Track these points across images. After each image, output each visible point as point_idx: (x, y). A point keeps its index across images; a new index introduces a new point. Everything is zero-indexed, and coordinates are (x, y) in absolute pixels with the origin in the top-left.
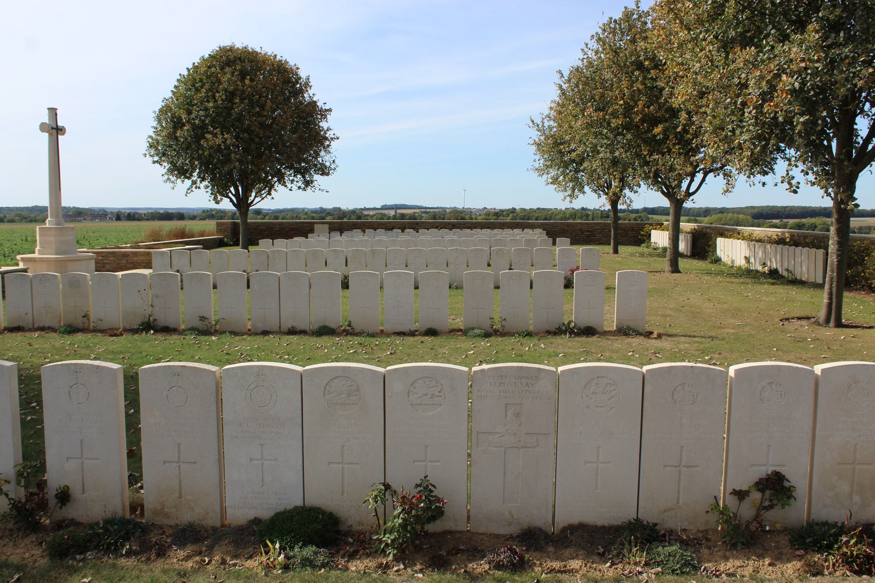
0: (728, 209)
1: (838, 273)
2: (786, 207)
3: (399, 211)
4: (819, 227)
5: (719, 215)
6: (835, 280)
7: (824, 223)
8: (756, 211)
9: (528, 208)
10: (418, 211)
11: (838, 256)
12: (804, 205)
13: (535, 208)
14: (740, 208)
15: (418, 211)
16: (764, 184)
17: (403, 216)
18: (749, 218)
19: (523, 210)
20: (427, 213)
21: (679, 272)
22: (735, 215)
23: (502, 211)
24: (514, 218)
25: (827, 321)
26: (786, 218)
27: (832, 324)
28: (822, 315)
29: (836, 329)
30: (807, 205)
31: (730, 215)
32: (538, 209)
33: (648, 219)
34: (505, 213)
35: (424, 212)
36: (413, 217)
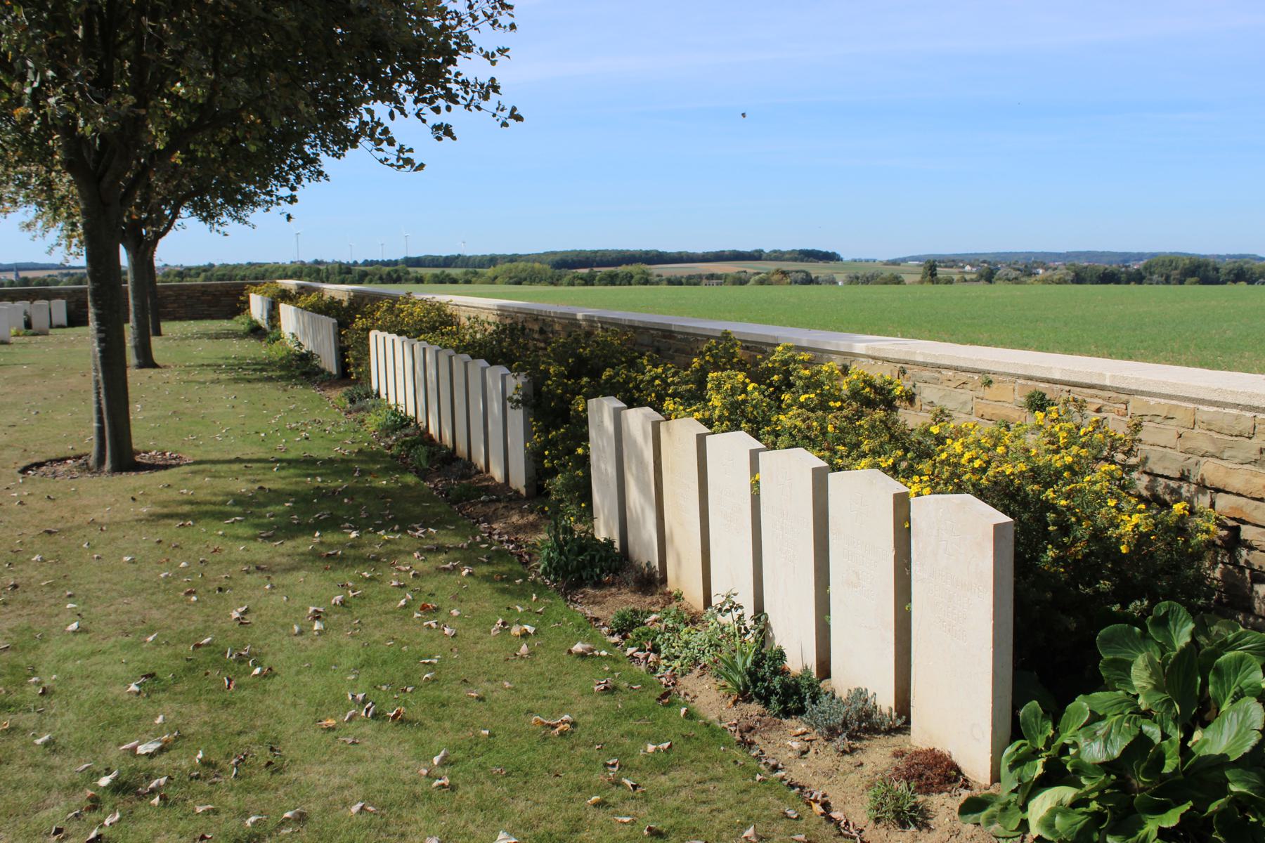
0: (520, 256)
1: (104, 372)
2: (596, 252)
3: (22, 274)
4: (637, 277)
5: (508, 265)
6: (102, 385)
7: (644, 272)
8: (558, 258)
9: (231, 262)
10: (55, 272)
11: (101, 341)
12: (619, 248)
13: (244, 262)
14: (538, 255)
15: (55, 272)
16: (289, 217)
17: (26, 281)
18: (547, 267)
19: (225, 266)
20: (72, 275)
21: (155, 366)
22: (530, 265)
23: (189, 269)
24: (207, 279)
25: (101, 460)
26: (598, 266)
27: (108, 466)
28: (90, 447)
29: (117, 477)
30: (625, 249)
31: (521, 265)
32: (249, 264)
33: (408, 273)
34: (193, 272)
35: (66, 275)
36: (43, 282)
